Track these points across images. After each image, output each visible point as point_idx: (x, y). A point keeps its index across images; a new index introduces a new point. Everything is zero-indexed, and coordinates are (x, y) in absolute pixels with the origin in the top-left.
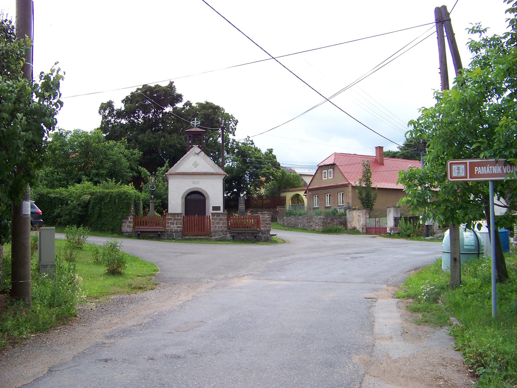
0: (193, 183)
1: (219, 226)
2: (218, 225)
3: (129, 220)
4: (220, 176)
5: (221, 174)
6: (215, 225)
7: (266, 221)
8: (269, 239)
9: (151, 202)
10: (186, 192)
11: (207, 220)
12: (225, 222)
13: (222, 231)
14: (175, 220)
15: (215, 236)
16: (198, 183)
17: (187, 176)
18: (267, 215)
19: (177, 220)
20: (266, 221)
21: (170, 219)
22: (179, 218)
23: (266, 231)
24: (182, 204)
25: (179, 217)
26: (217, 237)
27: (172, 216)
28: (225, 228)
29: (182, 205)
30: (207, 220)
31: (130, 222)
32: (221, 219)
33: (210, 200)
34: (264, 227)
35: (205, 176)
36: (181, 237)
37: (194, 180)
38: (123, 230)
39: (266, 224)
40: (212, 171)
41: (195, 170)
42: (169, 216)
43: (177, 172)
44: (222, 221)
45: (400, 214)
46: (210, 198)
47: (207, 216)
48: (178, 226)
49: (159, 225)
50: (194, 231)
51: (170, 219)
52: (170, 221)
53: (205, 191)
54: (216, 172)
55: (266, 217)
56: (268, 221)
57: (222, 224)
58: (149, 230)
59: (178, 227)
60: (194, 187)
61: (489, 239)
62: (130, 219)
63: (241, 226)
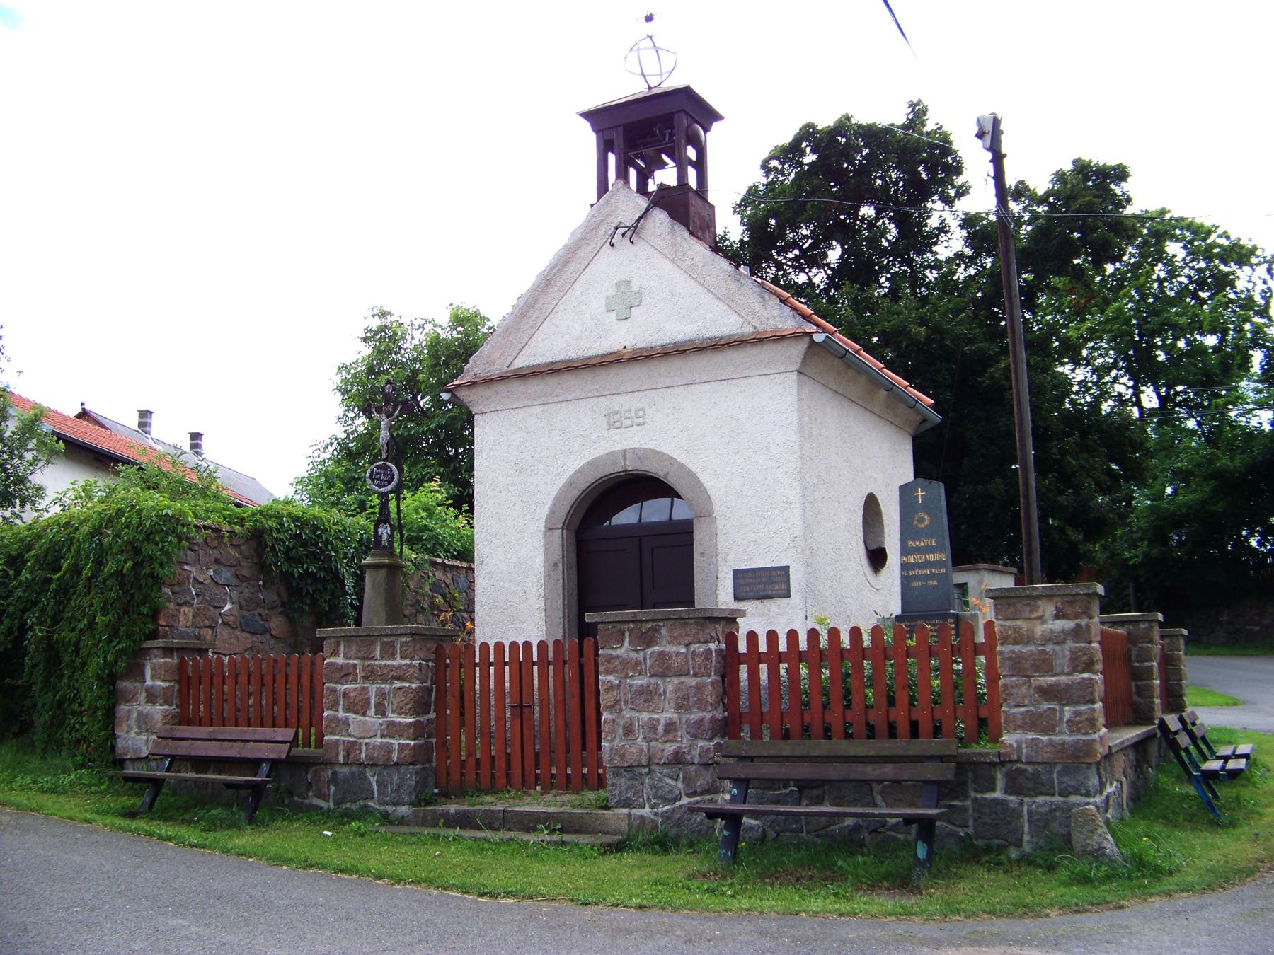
0: (612, 425)
1: (653, 726)
2: (645, 716)
3: (149, 682)
4: (769, 350)
5: (779, 338)
6: (628, 714)
7: (1044, 665)
8: (1078, 840)
9: (369, 566)
10: (570, 484)
11: (484, 677)
12: (699, 688)
13: (678, 760)
14: (370, 676)
15: (627, 804)
16: (640, 419)
17: (569, 380)
18: (1048, 609)
19: (385, 681)
20: (1044, 665)
21: (345, 674)
22: (398, 661)
23: (1049, 764)
24: (550, 566)
25: (393, 656)
26: (646, 811)
27: (354, 649)
28: (695, 737)
29: (548, 577)
30: (484, 677)
31: (152, 697)
32: (664, 668)
33: (720, 524)
34: (1033, 723)
35: (676, 363)
36: (416, 803)
37: (618, 403)
38: (120, 744)
39: (1048, 693)
40: (729, 324)
41: (621, 338)
42: (335, 653)
43: (520, 363)
44: (671, 684)
45: (180, 724)
46: (718, 508)
47: (752, 636)
48: (392, 724)
49: (57, 723)
50: (584, 748)
51: (345, 674)
52: (342, 687)
53: (681, 466)
54: (748, 330)
55: (1039, 629)
56: (1063, 662)
57: (679, 707)
58: (213, 750)
59: (392, 730)
60: (619, 447)
61: (670, 506)
62: (154, 677)
63: (835, 717)
